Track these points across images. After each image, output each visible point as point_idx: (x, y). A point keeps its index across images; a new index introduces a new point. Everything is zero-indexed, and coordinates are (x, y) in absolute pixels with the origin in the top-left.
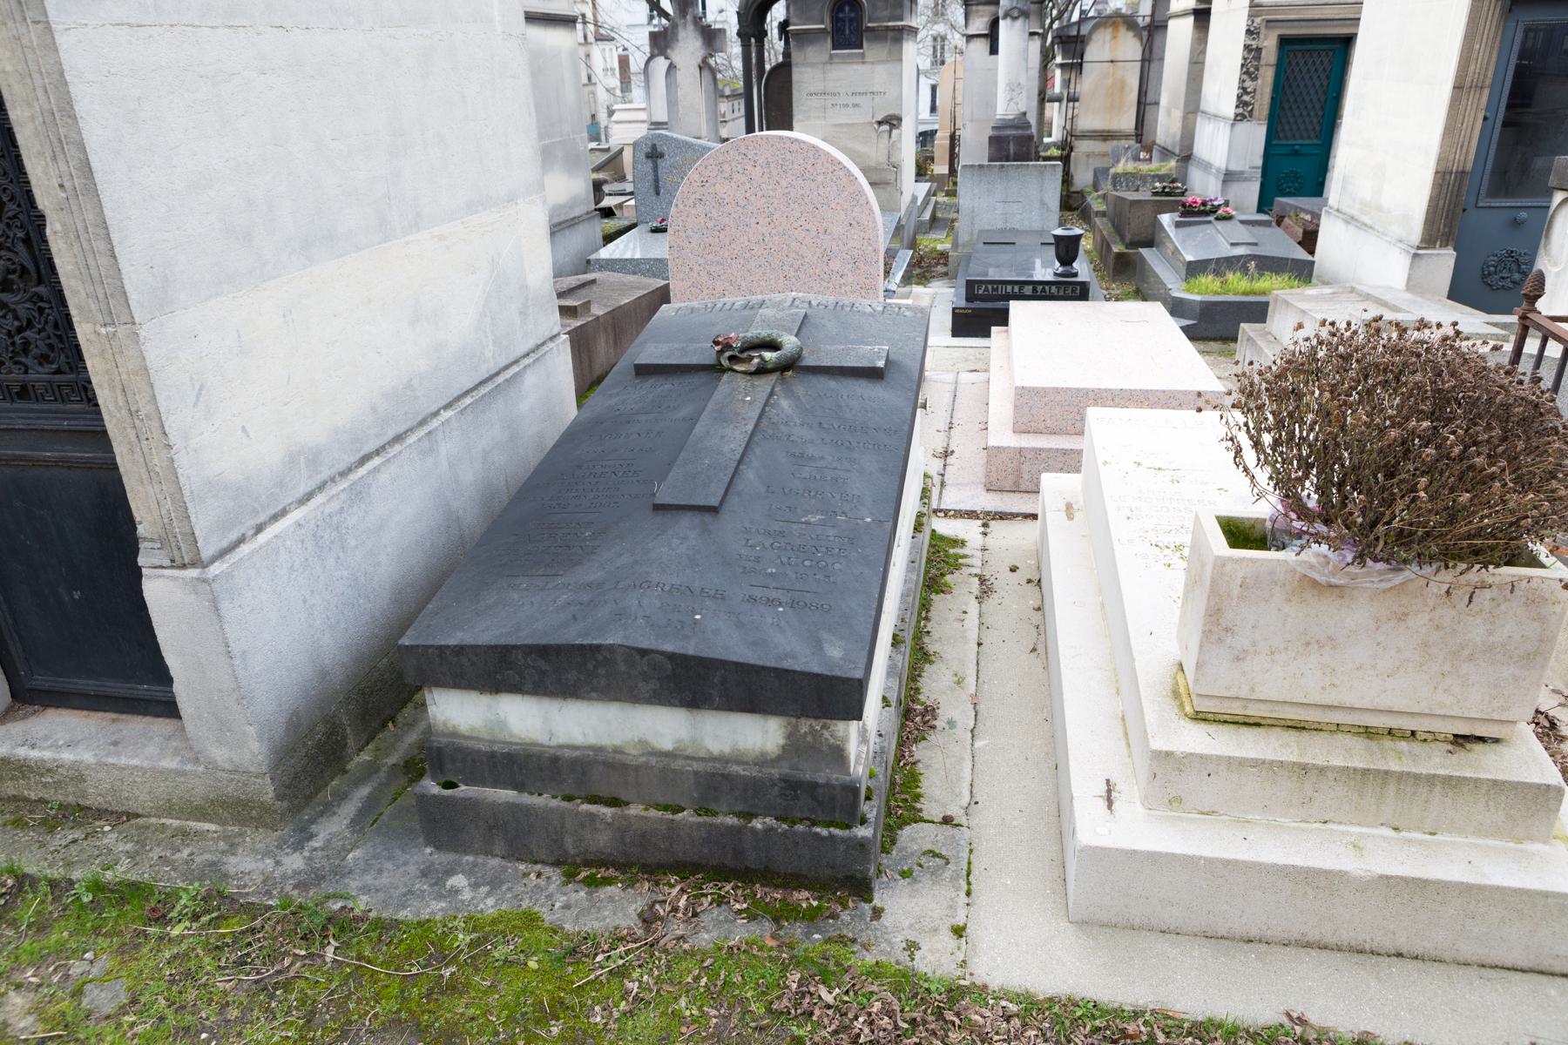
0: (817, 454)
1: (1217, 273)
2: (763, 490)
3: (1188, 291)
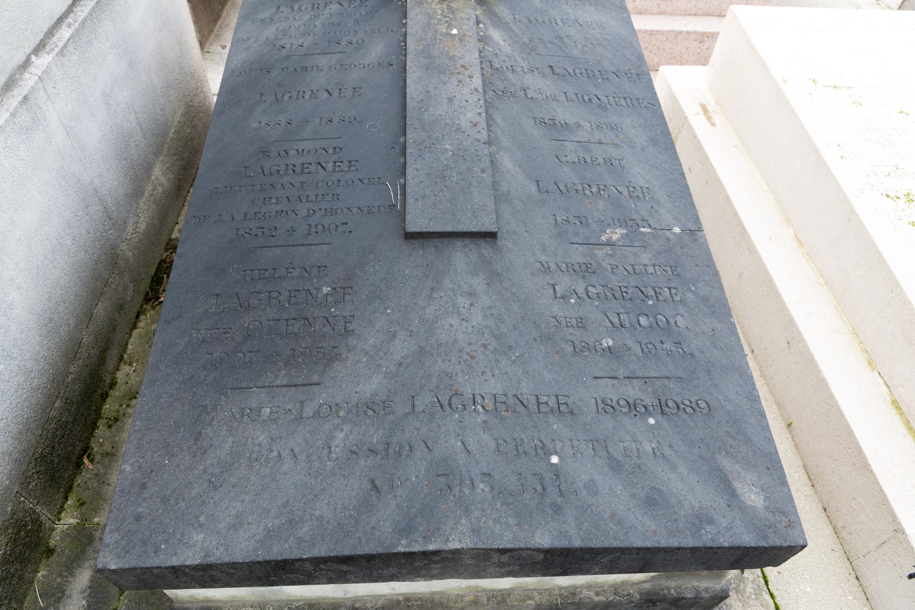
0: (570, 120)
2: (534, 189)
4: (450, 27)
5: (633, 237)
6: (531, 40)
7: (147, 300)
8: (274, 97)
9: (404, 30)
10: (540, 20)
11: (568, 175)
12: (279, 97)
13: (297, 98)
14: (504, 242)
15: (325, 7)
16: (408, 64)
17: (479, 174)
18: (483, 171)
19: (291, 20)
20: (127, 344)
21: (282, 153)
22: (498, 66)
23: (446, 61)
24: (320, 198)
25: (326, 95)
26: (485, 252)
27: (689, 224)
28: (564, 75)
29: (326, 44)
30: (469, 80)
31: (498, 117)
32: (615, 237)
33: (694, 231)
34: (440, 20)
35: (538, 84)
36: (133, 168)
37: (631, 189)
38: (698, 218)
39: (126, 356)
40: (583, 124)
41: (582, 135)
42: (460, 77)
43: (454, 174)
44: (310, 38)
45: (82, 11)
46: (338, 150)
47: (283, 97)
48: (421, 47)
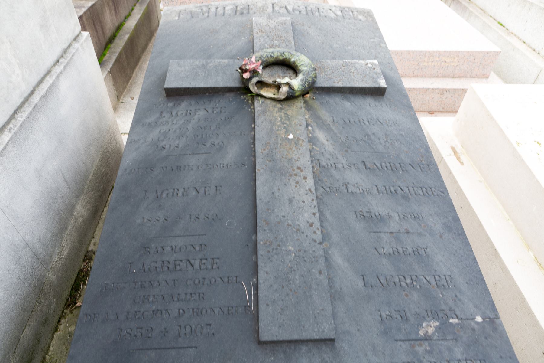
2: (361, 284)
4: (287, 132)
5: (444, 328)
7: (67, 305)
8: (155, 194)
9: (253, 133)
10: (352, 120)
11: (386, 267)
12: (159, 194)
13: (173, 196)
14: (342, 345)
15: (195, 113)
16: (257, 167)
17: (317, 276)
18: (320, 273)
20: (49, 347)
21: (160, 249)
22: (324, 164)
23: (286, 164)
24: (188, 297)
25: (194, 193)
26: (325, 356)
27: (488, 312)
28: (374, 169)
29: (195, 145)
30: (304, 181)
31: (327, 213)
32: (431, 331)
33: (493, 320)
34: (279, 126)
35: (356, 179)
36: (60, 213)
37: (437, 277)
38: (493, 305)
39: (47, 357)
40: (392, 214)
41: (394, 226)
42: (297, 178)
43: (297, 277)
44: (184, 140)
45: (22, 116)
46: (203, 247)
47: (162, 194)
48: (266, 151)
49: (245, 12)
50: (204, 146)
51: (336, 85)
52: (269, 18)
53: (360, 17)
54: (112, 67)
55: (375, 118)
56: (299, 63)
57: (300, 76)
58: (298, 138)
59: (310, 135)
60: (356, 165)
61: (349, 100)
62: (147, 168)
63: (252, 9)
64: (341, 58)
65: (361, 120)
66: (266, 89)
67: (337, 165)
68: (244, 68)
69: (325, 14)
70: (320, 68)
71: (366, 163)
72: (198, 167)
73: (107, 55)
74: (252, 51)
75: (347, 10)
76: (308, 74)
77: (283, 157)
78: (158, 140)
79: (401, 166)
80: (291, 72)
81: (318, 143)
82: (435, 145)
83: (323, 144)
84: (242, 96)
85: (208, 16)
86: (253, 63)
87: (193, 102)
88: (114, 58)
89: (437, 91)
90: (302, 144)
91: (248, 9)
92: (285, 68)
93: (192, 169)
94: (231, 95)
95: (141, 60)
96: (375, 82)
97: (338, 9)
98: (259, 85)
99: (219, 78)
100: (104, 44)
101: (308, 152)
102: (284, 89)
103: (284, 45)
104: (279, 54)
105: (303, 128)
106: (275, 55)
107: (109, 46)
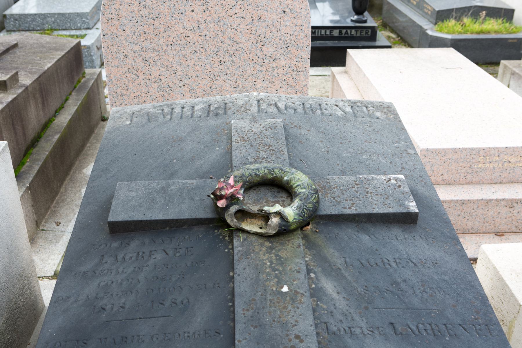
1: (458, 19)
3: (441, 31)
6: (366, 288)
10: (372, 261)
15: (150, 256)
16: (237, 337)
19: (114, 272)
22: (335, 329)
23: (278, 331)
34: (269, 274)
48: (250, 313)
49: (221, 112)
50: (161, 306)
51: (348, 211)
52: (254, 120)
53: (378, 114)
54: (32, 181)
55: (405, 256)
56: (294, 184)
57: (297, 202)
58: (296, 291)
59: (313, 286)
60: (381, 329)
61: (366, 232)
62: (78, 341)
63: (230, 108)
64: (354, 172)
65: (385, 261)
66: (249, 220)
67: (353, 330)
68: (218, 193)
69: (330, 111)
70: (324, 188)
71: (396, 326)
72: (152, 337)
73: (27, 164)
74: (229, 165)
75: (360, 105)
76: (307, 198)
77: (274, 321)
78: (96, 297)
79: (447, 327)
80: (284, 195)
81: (324, 297)
82: (507, 285)
83: (332, 299)
84: (216, 231)
85: (171, 119)
86: (231, 185)
87: (147, 241)
88: (37, 168)
89: (503, 203)
90: (301, 300)
91: (225, 108)
92: (276, 190)
93: (143, 342)
94: (200, 230)
95: (74, 168)
96: (402, 205)
97: (347, 104)
98: (239, 215)
99: (185, 206)
100: (24, 148)
101: (310, 312)
102: (275, 221)
103: (273, 157)
104: (266, 171)
105: (302, 276)
106: (261, 173)
107: (30, 151)
